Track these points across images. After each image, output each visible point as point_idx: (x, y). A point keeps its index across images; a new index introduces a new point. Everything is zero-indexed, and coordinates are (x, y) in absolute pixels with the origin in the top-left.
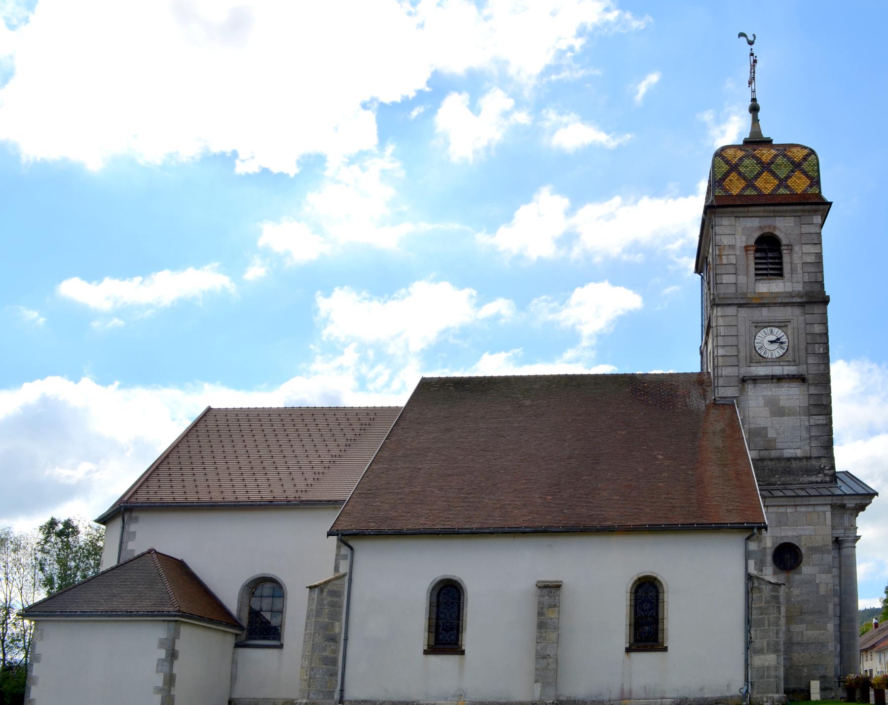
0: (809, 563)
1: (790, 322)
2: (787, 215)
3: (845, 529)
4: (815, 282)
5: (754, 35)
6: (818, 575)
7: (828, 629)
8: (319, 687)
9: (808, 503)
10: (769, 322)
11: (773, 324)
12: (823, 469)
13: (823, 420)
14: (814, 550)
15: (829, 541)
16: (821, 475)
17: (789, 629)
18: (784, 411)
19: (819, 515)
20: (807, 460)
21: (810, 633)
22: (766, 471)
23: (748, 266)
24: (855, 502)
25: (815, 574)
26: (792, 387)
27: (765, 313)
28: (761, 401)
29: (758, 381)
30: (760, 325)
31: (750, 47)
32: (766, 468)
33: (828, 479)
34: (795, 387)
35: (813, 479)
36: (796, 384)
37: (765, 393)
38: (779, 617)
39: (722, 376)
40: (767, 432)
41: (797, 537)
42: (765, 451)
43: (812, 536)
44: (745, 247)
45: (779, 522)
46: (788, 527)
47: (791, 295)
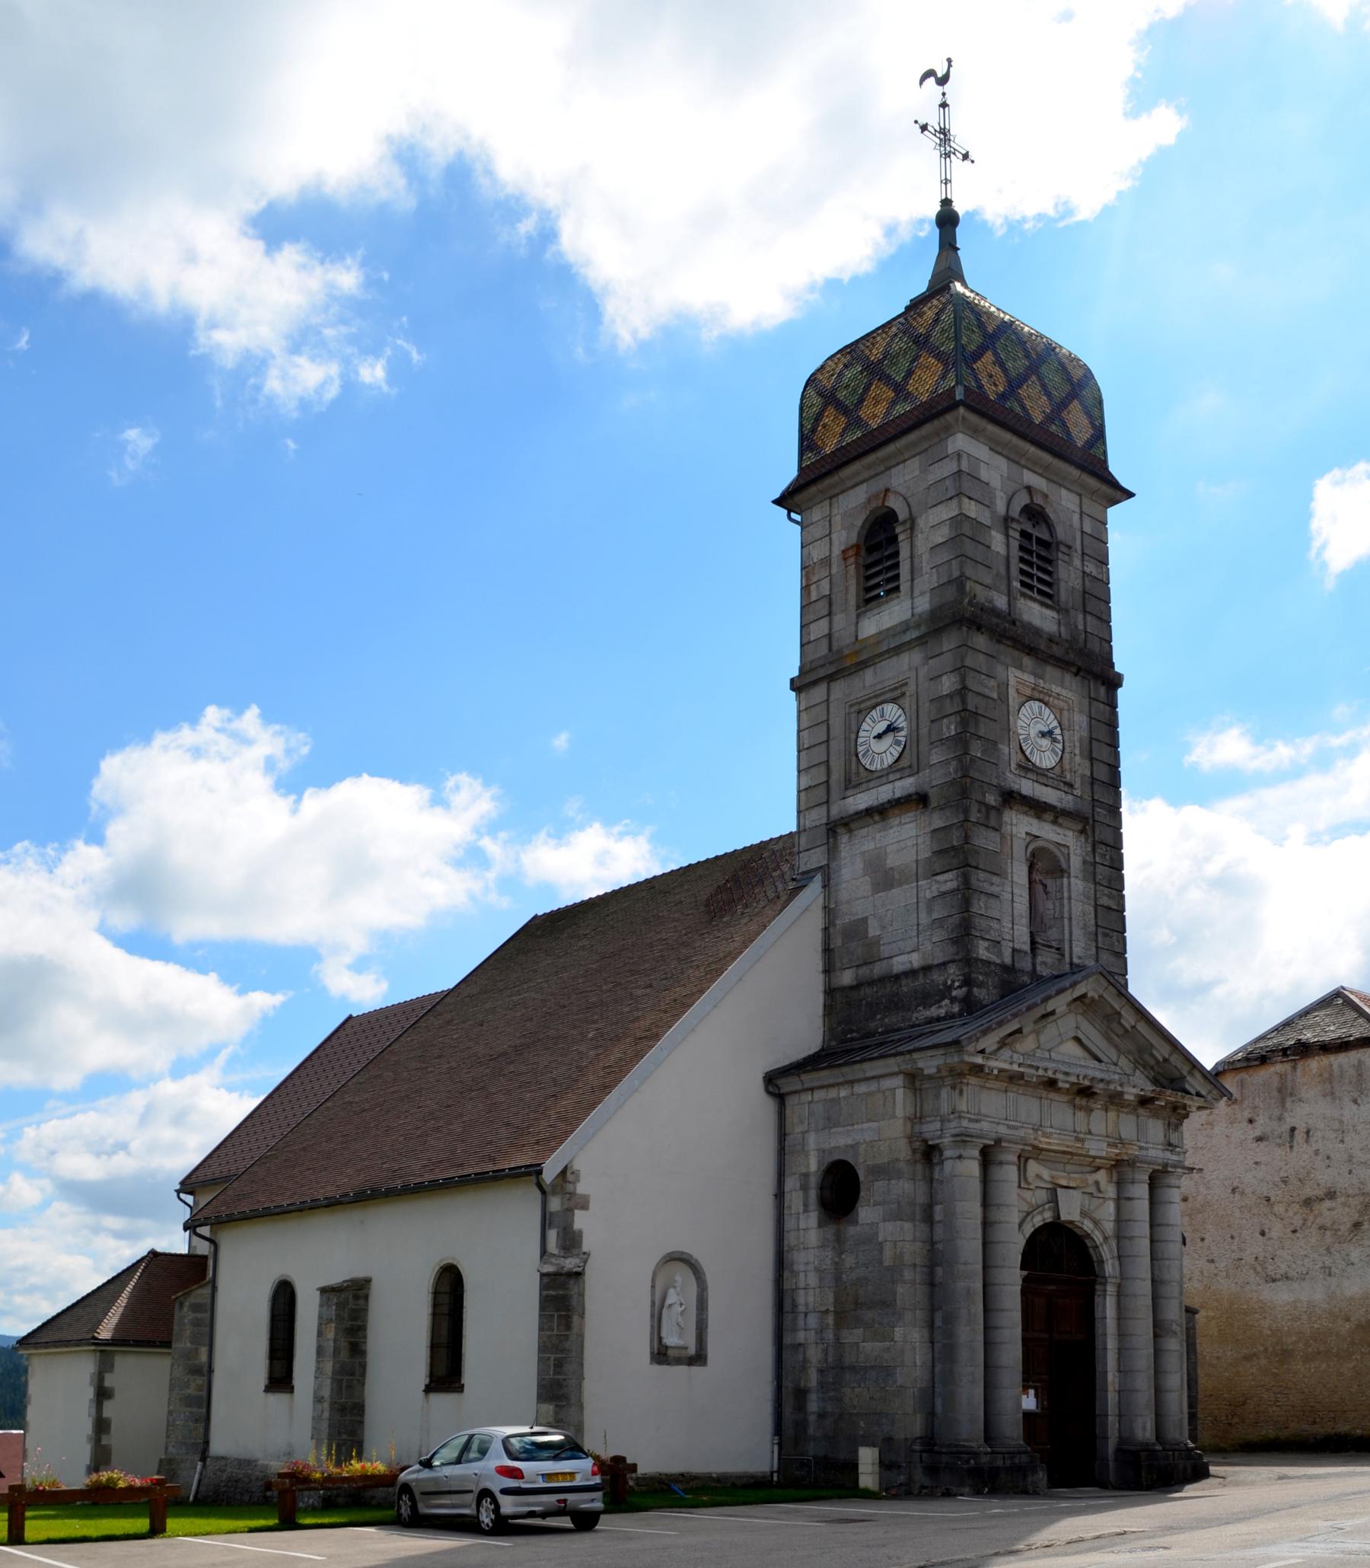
0: (869, 1201)
1: (906, 684)
2: (906, 457)
3: (942, 1121)
4: (949, 582)
5: (949, 61)
6: (881, 1225)
7: (896, 1339)
8: (180, 1437)
9: (863, 1076)
10: (876, 696)
12: (950, 988)
13: (951, 880)
14: (880, 1171)
15: (903, 1151)
16: (947, 1001)
17: (838, 1339)
19: (886, 1098)
21: (868, 1346)
22: (863, 1008)
23: (847, 589)
25: (877, 1223)
26: (906, 823)
28: (859, 865)
29: (853, 826)
30: (861, 710)
31: (940, 89)
32: (864, 1002)
33: (956, 1009)
34: (910, 822)
35: (934, 1011)
36: (911, 814)
37: (865, 848)
38: (567, 1335)
39: (805, 830)
40: (867, 927)
41: (852, 1146)
42: (864, 968)
43: (874, 1143)
44: (843, 551)
45: (828, 1119)
46: (840, 1129)
47: (905, 627)
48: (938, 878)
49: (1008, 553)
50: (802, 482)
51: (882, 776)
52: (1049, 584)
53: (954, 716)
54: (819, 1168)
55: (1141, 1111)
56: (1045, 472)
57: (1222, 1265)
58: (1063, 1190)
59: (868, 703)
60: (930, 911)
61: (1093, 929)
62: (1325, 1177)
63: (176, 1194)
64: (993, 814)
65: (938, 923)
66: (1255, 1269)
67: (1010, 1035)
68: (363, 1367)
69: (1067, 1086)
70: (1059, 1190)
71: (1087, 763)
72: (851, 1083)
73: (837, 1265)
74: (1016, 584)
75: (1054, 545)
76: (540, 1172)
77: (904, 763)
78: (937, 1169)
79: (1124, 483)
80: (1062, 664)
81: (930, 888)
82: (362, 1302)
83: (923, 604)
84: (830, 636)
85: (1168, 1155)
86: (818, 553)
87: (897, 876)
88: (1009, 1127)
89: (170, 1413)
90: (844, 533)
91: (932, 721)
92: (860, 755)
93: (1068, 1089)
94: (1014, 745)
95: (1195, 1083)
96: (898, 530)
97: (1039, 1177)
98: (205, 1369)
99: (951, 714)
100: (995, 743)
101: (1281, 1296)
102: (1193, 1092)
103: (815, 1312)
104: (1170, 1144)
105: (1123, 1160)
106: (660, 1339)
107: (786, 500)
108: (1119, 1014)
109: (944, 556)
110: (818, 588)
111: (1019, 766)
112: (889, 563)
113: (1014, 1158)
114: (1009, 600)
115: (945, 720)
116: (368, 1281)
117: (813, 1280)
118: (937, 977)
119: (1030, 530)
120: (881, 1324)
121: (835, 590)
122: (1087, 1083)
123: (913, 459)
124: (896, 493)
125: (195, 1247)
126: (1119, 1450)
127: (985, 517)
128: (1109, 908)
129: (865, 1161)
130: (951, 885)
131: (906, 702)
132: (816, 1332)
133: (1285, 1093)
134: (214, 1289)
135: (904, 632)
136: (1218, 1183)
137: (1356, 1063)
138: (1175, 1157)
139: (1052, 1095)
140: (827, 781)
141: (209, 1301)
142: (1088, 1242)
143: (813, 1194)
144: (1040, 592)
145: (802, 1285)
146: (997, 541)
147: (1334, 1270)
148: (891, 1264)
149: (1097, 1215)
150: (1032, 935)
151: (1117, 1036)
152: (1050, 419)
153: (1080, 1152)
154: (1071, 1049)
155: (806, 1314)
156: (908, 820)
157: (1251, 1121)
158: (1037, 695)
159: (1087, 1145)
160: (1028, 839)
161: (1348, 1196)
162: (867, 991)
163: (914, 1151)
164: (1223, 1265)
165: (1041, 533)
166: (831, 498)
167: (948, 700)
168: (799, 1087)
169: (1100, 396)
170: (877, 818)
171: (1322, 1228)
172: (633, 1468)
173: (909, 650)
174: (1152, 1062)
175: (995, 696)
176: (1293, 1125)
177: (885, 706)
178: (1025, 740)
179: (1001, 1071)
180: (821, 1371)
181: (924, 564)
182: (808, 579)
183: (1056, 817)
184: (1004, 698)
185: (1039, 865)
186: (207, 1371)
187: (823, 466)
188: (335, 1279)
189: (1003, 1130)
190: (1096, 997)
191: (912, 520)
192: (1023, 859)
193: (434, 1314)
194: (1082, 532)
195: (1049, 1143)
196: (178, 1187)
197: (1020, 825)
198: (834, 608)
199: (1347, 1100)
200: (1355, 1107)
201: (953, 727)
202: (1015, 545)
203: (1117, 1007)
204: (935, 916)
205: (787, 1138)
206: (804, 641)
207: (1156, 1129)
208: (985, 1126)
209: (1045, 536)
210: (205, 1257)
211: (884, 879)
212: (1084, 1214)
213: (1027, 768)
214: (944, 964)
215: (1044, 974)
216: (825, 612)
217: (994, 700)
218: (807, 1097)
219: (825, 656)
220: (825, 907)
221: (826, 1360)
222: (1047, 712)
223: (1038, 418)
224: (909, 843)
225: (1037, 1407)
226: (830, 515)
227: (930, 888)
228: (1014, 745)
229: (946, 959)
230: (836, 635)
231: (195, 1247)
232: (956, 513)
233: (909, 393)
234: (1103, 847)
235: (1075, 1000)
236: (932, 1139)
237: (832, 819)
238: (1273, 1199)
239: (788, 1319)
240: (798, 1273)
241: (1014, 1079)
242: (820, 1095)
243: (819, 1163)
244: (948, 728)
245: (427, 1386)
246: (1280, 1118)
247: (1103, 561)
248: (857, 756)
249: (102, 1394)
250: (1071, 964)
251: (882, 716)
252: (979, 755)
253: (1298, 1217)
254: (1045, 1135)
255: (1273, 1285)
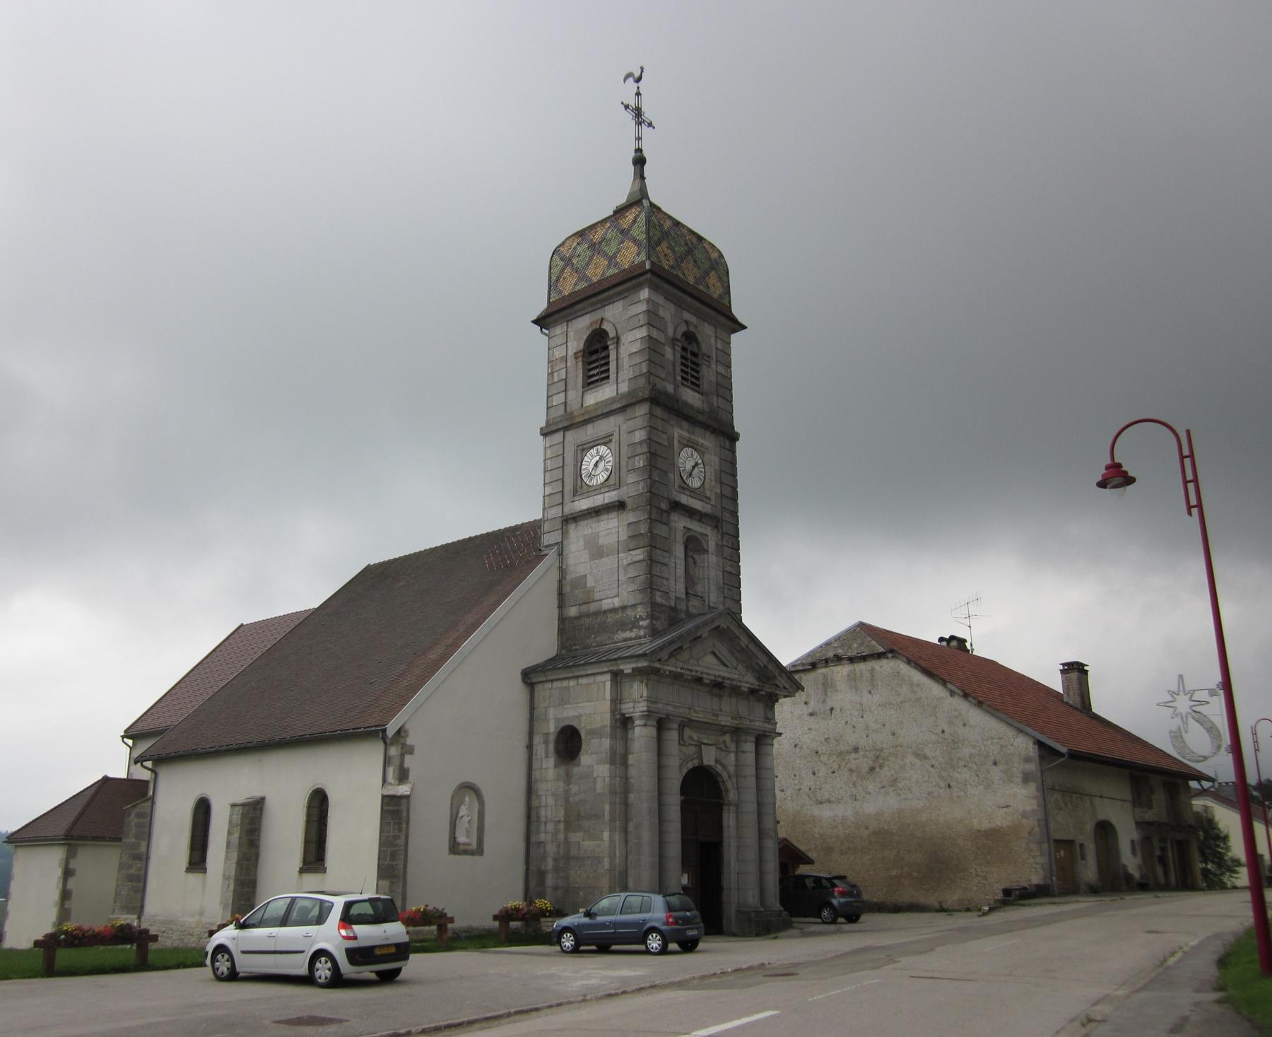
0: (588, 751)
4: (640, 375)
5: (642, 69)
6: (595, 767)
7: (604, 839)
10: (594, 441)
11: (598, 442)
14: (594, 733)
18: (603, 550)
20: (622, 611)
22: (583, 630)
24: (634, 665)
25: (593, 766)
27: (591, 431)
28: (582, 543)
30: (584, 448)
31: (636, 85)
36: (615, 513)
37: (586, 533)
41: (577, 717)
44: (575, 354)
46: (569, 706)
48: (631, 552)
49: (674, 359)
50: (551, 311)
51: (596, 490)
52: (697, 379)
53: (642, 456)
54: (555, 731)
55: (751, 698)
56: (696, 313)
57: (788, 793)
58: (705, 746)
59: (588, 445)
60: (626, 571)
61: (722, 585)
62: (851, 739)
63: (121, 738)
64: (665, 514)
65: (632, 579)
66: (809, 796)
67: (675, 650)
68: (257, 856)
69: (708, 682)
70: (703, 746)
71: (718, 485)
72: (577, 677)
73: (567, 792)
74: (679, 378)
75: (700, 356)
76: (384, 731)
77: (611, 482)
78: (630, 732)
79: (741, 318)
80: (706, 427)
81: (626, 558)
82: (258, 812)
83: (624, 388)
84: (565, 403)
85: (766, 725)
86: (559, 353)
87: (605, 550)
88: (675, 707)
89: (118, 886)
90: (575, 343)
91: (629, 458)
92: (583, 476)
93: (708, 684)
94: (677, 473)
95: (782, 681)
96: (609, 343)
97: (691, 738)
98: (145, 857)
99: (640, 454)
100: (666, 472)
101: (826, 813)
102: (781, 686)
103: (552, 821)
104: (767, 718)
105: (740, 728)
106: (455, 838)
107: (543, 322)
108: (739, 638)
109: (637, 360)
110: (558, 374)
111: (680, 486)
112: (603, 362)
113: (676, 726)
114: (675, 388)
115: (637, 458)
116: (263, 799)
117: (551, 801)
118: (630, 612)
119: (686, 346)
120: (594, 829)
121: (569, 376)
122: (720, 680)
123: (619, 302)
124: (608, 321)
125: (132, 774)
126: (739, 912)
127: (661, 338)
128: (731, 573)
129: (585, 726)
130: (641, 557)
131: (612, 445)
132: (552, 835)
133: (827, 686)
134: (153, 803)
135: (612, 403)
136: (786, 741)
137: (870, 668)
138: (770, 726)
139: (699, 687)
140: (562, 491)
141: (149, 811)
142: (719, 779)
143: (551, 746)
144: (692, 383)
145: (543, 804)
146: (668, 352)
147: (858, 797)
148: (602, 791)
149: (724, 762)
150: (686, 588)
151: (738, 651)
152: (698, 281)
153: (715, 722)
154: (710, 659)
155: (546, 823)
156: (613, 516)
157: (806, 703)
158: (690, 444)
159: (719, 719)
160: (685, 530)
161: (866, 751)
162: (586, 620)
163: (616, 721)
164: (789, 792)
165: (694, 348)
166: (568, 321)
167: (639, 446)
168: (544, 679)
169: (728, 269)
170: (593, 515)
171: (851, 771)
172: (452, 920)
173: (615, 414)
174: (757, 668)
175: (666, 444)
176: (832, 706)
177: (599, 447)
178: (683, 471)
179: (670, 672)
180: (555, 860)
181: (625, 364)
182: (552, 369)
183: (701, 518)
184: (671, 446)
185: (690, 546)
186: (144, 858)
187: (563, 302)
188: (241, 799)
189: (670, 708)
190: (725, 627)
191: (617, 340)
192: (682, 542)
193: (308, 822)
194: (717, 348)
195: (697, 717)
196: (123, 734)
197: (680, 523)
198: (568, 387)
199: (865, 693)
200: (870, 696)
201: (641, 462)
202: (678, 355)
203: (737, 633)
204: (629, 576)
205: (535, 711)
206: (550, 405)
207: (759, 709)
208: (660, 706)
209: (696, 350)
210: (147, 782)
211: (597, 552)
212: (717, 761)
213: (684, 488)
214: (634, 606)
215: (694, 612)
216: (563, 389)
217: (665, 446)
218: (549, 685)
219: (563, 416)
220: (560, 568)
221: (558, 853)
222: (696, 454)
223: (691, 280)
224: (614, 531)
225: (688, 882)
226: (567, 331)
227: (626, 558)
228: (677, 473)
229: (636, 602)
230: (569, 403)
231: (132, 774)
232: (645, 335)
233: (617, 263)
234: (728, 536)
235: (713, 629)
236: (628, 713)
237: (565, 514)
238: (820, 752)
239: (534, 826)
240: (540, 796)
241: (676, 677)
242: (557, 684)
243: (556, 727)
244: (639, 463)
245: (300, 868)
246: (824, 701)
247: (729, 366)
248: (581, 476)
249: (68, 873)
250: (709, 606)
251: (597, 453)
252: (657, 479)
253: (836, 763)
254: (695, 711)
255: (820, 806)
